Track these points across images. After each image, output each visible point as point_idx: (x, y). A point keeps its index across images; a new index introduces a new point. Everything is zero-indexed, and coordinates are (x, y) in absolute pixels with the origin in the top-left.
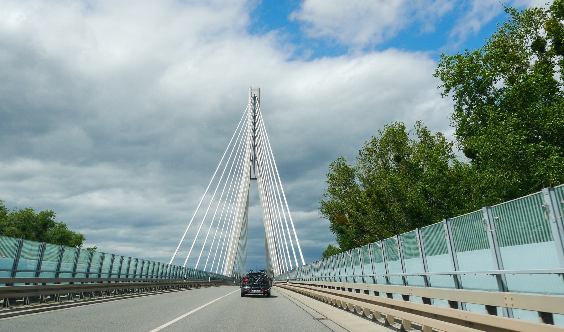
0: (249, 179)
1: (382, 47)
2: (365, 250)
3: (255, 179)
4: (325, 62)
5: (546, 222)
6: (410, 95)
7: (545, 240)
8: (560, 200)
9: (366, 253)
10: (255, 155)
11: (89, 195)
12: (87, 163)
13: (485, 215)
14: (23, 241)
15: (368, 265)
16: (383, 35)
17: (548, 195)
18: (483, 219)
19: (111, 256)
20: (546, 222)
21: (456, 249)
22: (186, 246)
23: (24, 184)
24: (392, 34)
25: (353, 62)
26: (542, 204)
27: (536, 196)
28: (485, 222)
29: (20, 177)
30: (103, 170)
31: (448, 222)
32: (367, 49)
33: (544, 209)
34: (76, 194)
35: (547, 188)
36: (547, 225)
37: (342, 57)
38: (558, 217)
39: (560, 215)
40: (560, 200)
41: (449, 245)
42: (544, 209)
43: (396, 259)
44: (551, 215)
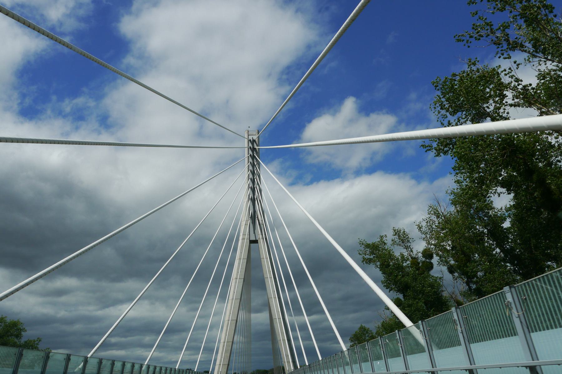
0: (246, 242)
1: (371, 170)
2: (364, 348)
3: (256, 242)
4: (322, 185)
5: (510, 318)
6: (394, 210)
7: (554, 326)
8: (521, 297)
9: (395, 342)
10: (255, 211)
11: (120, 307)
12: (118, 279)
13: (455, 315)
14: (22, 350)
15: (458, 348)
16: (372, 159)
17: (510, 293)
18: (506, 301)
19: (110, 362)
20: (510, 318)
21: (531, 327)
22: (194, 348)
23: (63, 299)
24: (379, 158)
25: (346, 184)
26: (505, 302)
27: (529, 285)
28: (508, 306)
29: (60, 293)
30: (130, 284)
31: (424, 322)
32: (359, 172)
33: (507, 306)
34: (108, 306)
35: (508, 287)
36: (510, 320)
37: (337, 180)
38: (521, 313)
39: (522, 310)
40: (521, 297)
41: (400, 348)
42: (507, 306)
43: (367, 361)
44: (514, 311)
